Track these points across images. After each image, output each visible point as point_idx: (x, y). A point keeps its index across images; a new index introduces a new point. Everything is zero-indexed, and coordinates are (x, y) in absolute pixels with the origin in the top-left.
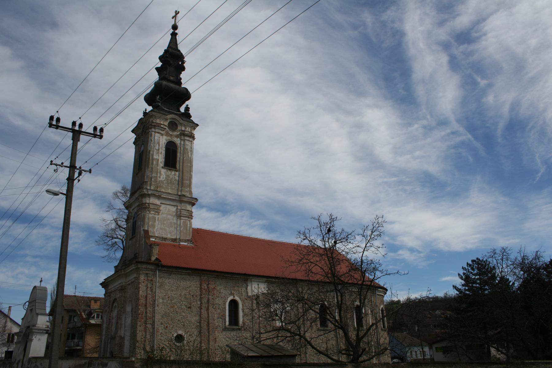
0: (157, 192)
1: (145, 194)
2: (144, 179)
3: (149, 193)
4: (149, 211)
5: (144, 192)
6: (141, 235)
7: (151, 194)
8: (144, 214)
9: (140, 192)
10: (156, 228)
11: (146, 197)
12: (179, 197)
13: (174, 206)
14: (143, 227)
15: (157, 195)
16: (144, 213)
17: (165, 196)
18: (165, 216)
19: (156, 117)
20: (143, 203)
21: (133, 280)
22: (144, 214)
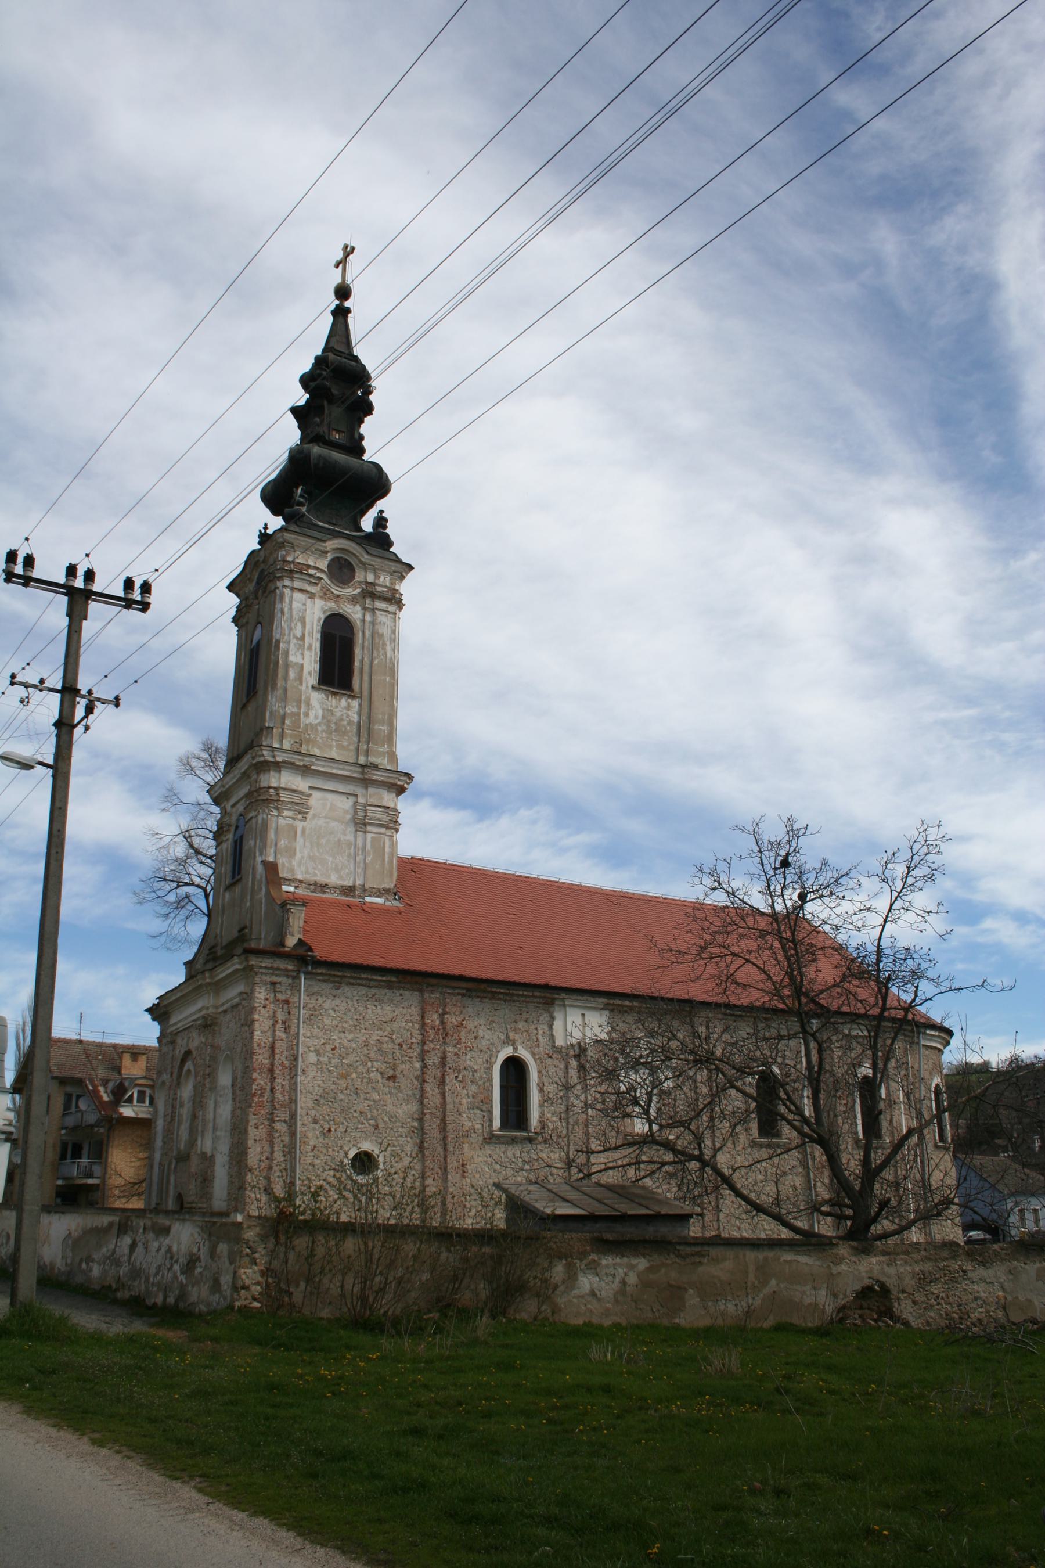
0: (300, 757)
1: (266, 762)
2: (263, 720)
3: (279, 759)
4: (277, 809)
5: (263, 755)
6: (258, 877)
7: (284, 762)
8: (263, 819)
9: (253, 758)
10: (298, 855)
11: (269, 771)
12: (360, 770)
13: (348, 795)
14: (261, 854)
15: (299, 766)
16: (265, 816)
17: (323, 766)
18: (321, 822)
19: (293, 547)
20: (261, 788)
21: (237, 1000)
22: (263, 819)
